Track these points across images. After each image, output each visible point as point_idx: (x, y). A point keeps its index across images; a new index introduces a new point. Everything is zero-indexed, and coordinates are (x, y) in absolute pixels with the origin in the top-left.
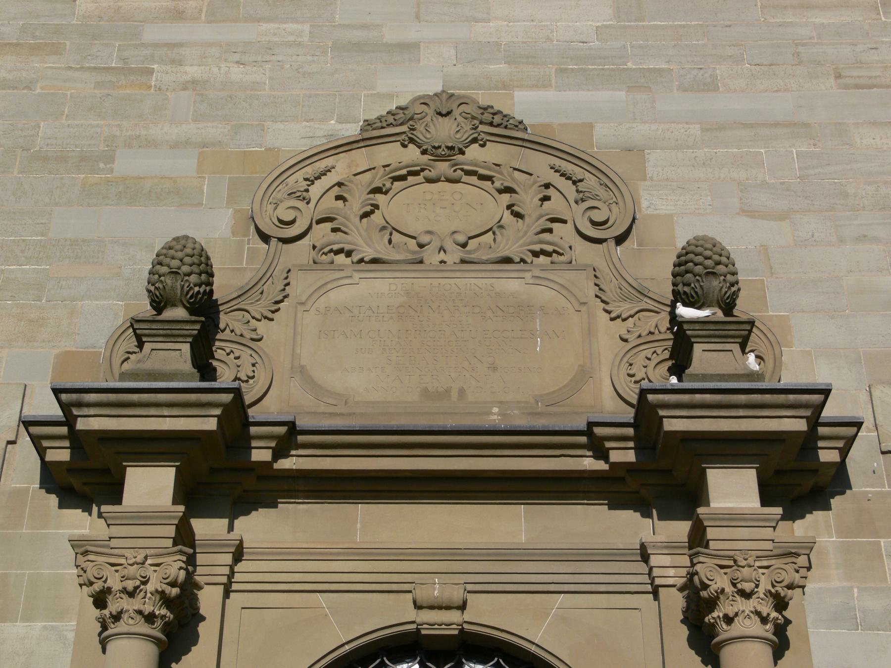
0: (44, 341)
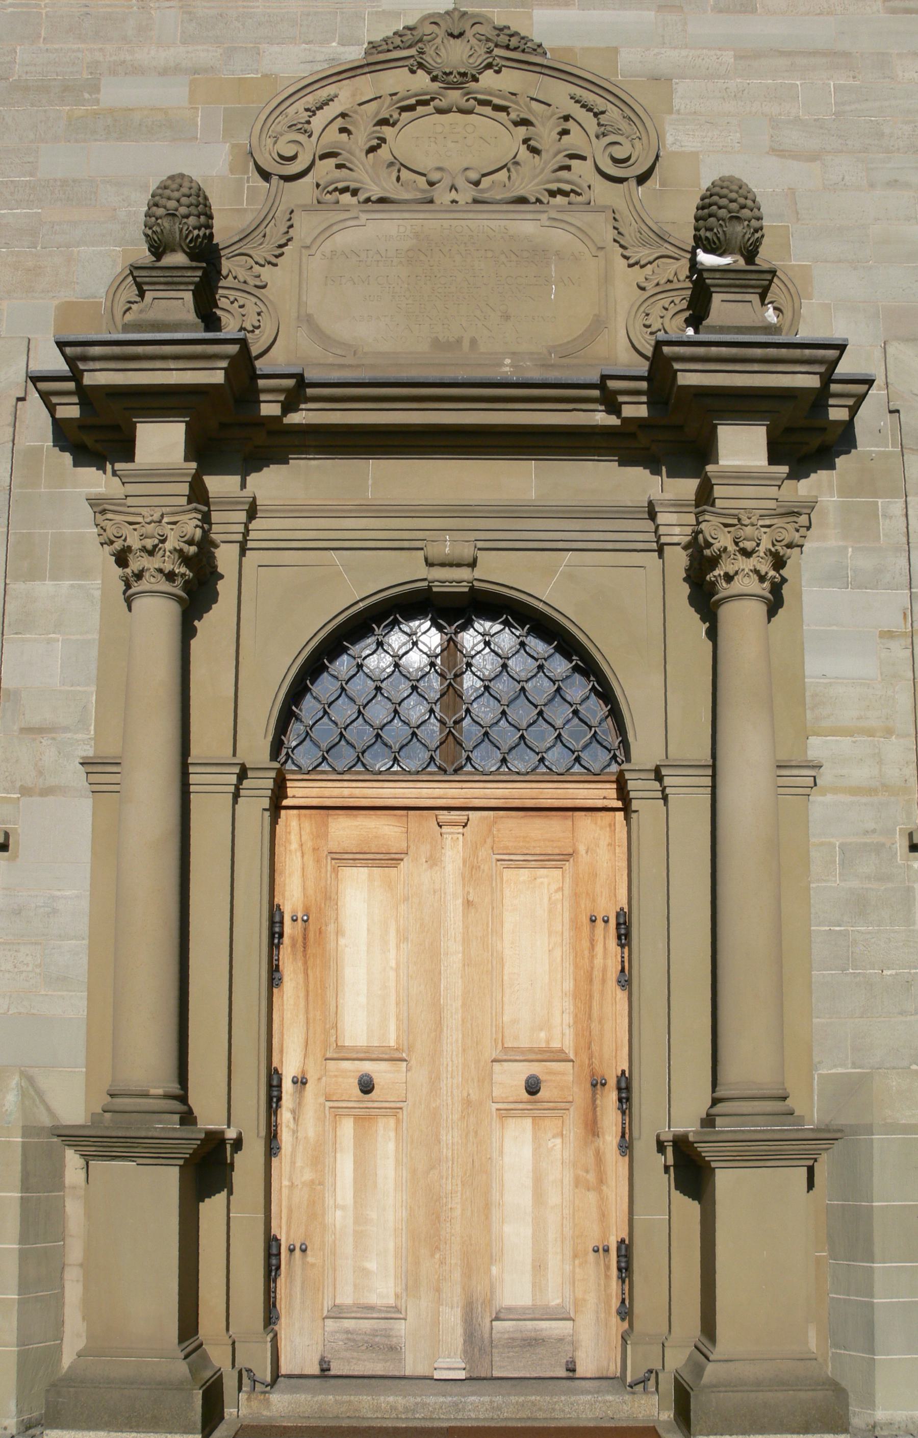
0: (43, 292)
